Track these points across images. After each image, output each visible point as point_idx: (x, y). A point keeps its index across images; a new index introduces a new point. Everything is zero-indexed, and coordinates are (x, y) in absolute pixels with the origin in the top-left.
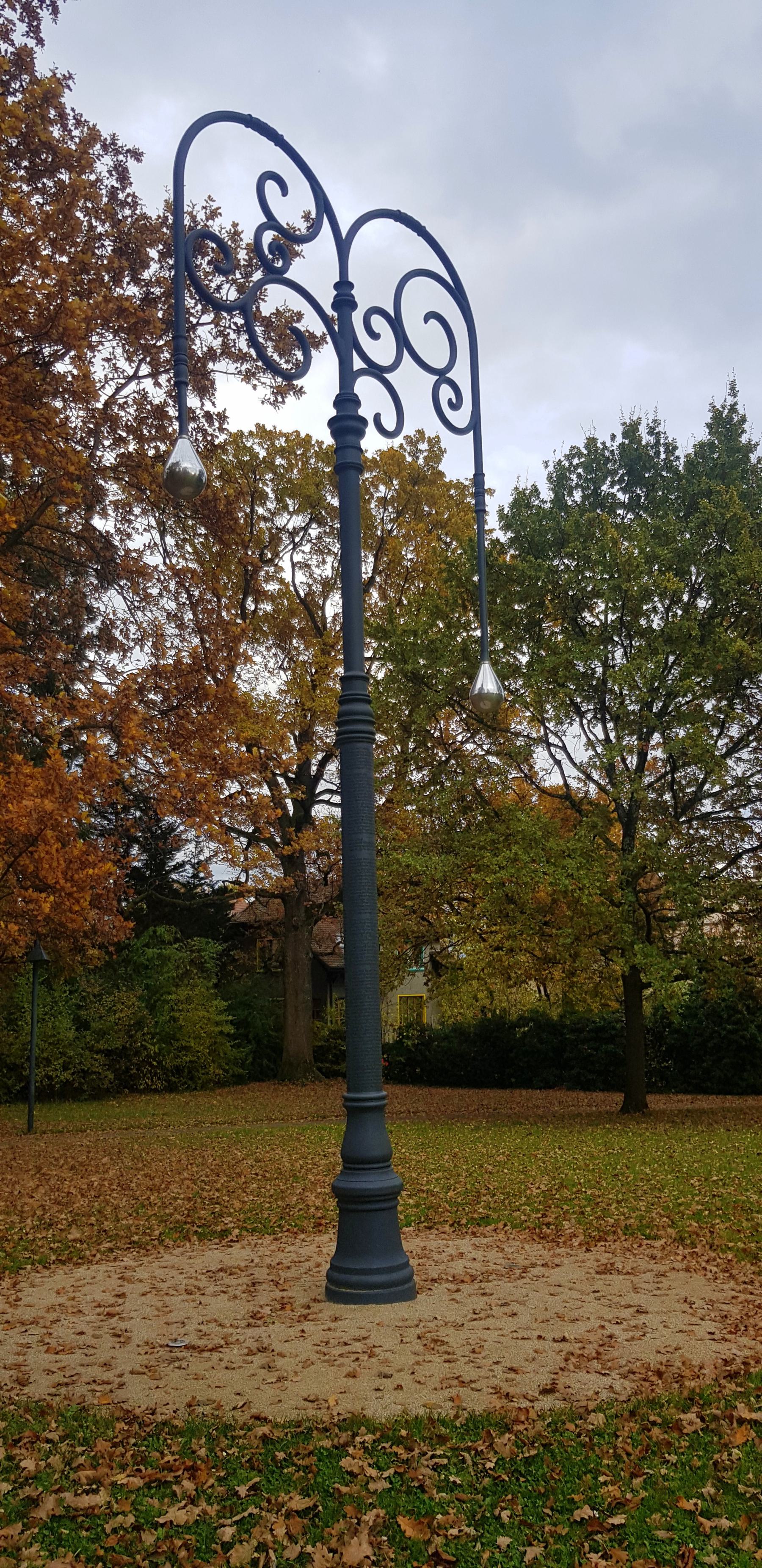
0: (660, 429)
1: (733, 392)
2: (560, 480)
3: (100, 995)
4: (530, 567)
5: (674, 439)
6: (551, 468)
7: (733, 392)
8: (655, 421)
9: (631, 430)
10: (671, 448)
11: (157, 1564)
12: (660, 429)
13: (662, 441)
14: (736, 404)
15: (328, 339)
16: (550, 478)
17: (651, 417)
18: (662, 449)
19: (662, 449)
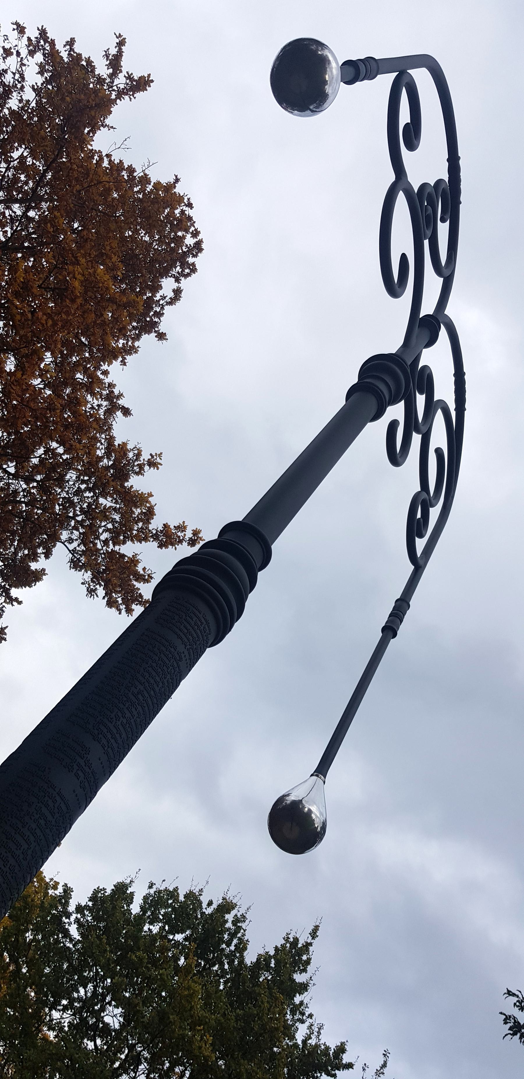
0: (244, 925)
1: (314, 933)
2: (155, 901)
3: (111, 247)
4: (98, 946)
5: (247, 941)
6: (152, 891)
7: (314, 933)
8: (243, 916)
9: (226, 907)
10: (242, 947)
11: (3, 226)
12: (244, 925)
13: (239, 935)
14: (311, 944)
15: (138, 610)
16: (145, 898)
17: (242, 911)
18: (235, 941)
19: (235, 941)
